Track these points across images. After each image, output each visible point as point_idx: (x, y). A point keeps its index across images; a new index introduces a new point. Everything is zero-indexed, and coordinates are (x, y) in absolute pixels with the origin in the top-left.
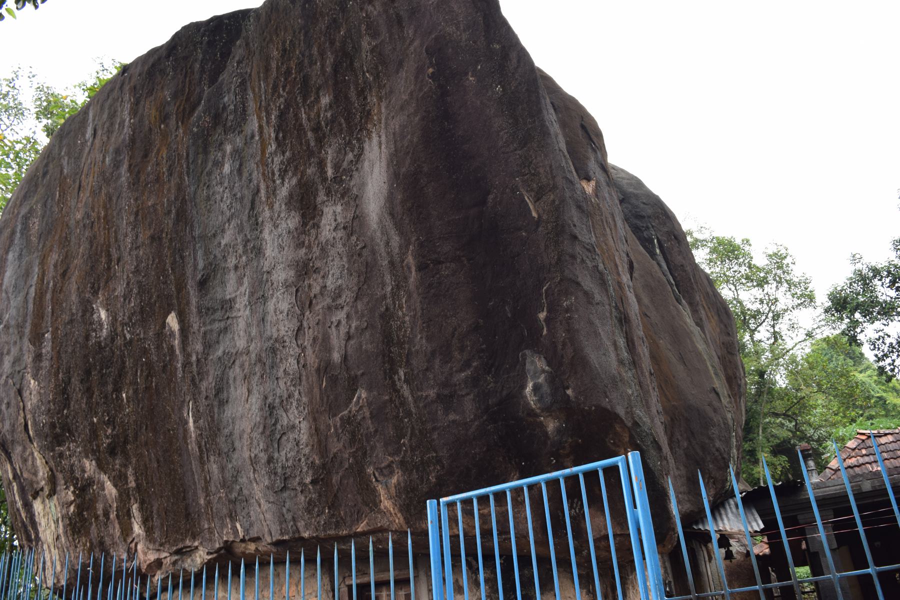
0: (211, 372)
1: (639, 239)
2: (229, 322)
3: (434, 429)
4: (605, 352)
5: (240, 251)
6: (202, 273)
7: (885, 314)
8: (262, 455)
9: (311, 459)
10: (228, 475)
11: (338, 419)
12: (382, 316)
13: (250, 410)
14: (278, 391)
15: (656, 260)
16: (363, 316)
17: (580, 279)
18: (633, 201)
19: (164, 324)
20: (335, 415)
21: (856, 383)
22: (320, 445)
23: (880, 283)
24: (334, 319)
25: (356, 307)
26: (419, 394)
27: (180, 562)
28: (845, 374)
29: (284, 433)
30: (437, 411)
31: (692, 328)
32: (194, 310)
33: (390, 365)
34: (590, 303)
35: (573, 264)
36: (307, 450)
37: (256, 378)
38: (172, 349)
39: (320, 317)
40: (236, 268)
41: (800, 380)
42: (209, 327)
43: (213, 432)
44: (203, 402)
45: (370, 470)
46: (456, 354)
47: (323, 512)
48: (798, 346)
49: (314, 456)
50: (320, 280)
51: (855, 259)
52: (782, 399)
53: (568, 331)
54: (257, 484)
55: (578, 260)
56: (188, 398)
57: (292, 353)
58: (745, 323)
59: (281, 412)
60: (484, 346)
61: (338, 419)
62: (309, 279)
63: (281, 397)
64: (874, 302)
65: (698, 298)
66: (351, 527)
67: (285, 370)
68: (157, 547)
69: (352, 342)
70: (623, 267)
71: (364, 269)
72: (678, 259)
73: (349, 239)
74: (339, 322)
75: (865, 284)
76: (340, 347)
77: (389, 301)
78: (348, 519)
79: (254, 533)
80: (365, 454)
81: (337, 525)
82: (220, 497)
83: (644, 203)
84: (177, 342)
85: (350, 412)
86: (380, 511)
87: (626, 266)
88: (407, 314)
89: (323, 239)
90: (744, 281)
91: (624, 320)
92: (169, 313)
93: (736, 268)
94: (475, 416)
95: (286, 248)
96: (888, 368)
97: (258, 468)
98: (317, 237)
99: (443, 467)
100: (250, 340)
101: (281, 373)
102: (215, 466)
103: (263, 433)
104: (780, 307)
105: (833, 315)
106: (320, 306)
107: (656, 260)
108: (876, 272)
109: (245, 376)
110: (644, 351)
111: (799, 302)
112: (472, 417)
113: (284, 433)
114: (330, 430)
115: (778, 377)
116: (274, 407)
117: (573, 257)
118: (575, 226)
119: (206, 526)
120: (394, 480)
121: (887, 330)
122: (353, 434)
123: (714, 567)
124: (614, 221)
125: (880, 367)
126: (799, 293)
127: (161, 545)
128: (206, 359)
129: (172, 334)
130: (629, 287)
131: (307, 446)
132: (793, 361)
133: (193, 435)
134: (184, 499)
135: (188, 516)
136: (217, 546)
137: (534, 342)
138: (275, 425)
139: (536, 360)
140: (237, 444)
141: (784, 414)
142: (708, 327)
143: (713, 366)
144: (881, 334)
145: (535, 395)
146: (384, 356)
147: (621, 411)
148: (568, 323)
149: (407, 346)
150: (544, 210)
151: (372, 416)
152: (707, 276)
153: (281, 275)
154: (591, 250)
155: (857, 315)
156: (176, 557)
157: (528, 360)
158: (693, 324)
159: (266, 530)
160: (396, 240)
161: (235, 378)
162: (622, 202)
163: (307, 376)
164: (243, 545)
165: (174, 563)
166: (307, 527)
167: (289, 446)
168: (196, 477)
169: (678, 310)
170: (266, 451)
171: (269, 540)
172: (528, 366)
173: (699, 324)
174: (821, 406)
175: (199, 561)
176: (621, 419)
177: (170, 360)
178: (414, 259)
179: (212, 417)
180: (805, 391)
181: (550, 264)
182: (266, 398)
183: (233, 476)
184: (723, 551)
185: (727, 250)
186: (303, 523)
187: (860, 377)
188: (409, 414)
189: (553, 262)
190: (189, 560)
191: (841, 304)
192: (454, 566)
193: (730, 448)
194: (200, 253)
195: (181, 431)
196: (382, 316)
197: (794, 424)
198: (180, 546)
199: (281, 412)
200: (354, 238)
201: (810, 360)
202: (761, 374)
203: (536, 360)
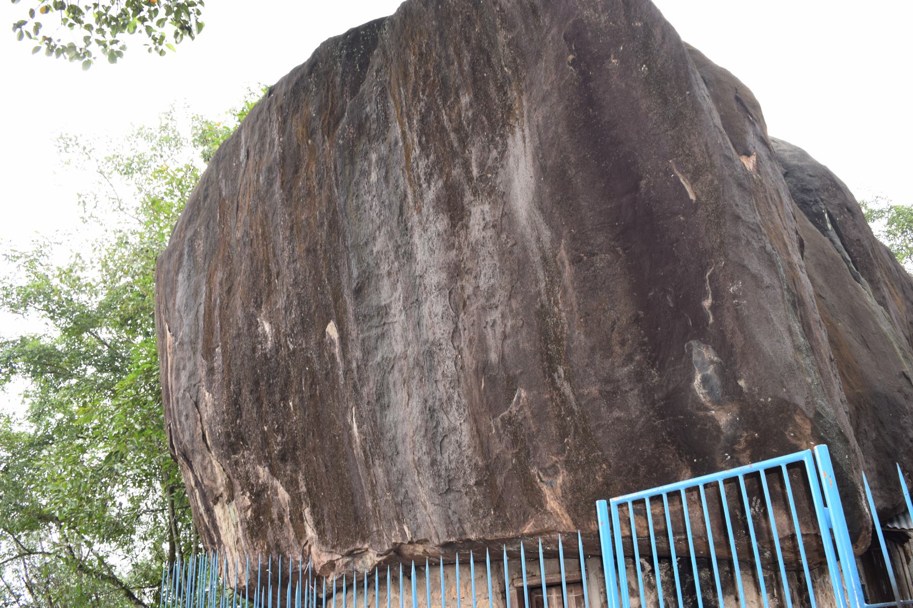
0: (372, 378)
1: (807, 214)
2: (386, 327)
3: (599, 427)
4: (779, 339)
5: (392, 258)
8: (425, 457)
10: (393, 479)
12: (538, 314)
13: (411, 413)
14: (438, 394)
17: (746, 262)
18: (798, 174)
19: (324, 333)
22: (482, 447)
24: (489, 319)
25: (511, 306)
26: (581, 391)
27: (352, 564)
29: (446, 436)
31: (874, 308)
32: (352, 318)
33: (550, 363)
35: (737, 246)
36: (469, 452)
37: (415, 382)
38: (333, 357)
40: (389, 274)
43: (376, 436)
44: (365, 408)
45: (534, 471)
46: (617, 349)
49: (477, 458)
53: (737, 318)
55: (743, 242)
57: (449, 355)
59: (441, 415)
60: (646, 339)
61: (498, 420)
62: (462, 280)
63: (440, 400)
65: (879, 274)
66: (517, 529)
69: (509, 341)
71: (516, 266)
72: (853, 233)
73: (499, 237)
74: (494, 322)
76: (497, 347)
77: (544, 297)
78: (515, 520)
79: (421, 536)
81: (504, 527)
82: (387, 501)
83: (811, 176)
84: (337, 350)
86: (546, 512)
87: (796, 245)
88: (565, 309)
89: (472, 239)
91: (797, 303)
94: (641, 412)
95: (437, 251)
97: (421, 471)
98: (466, 238)
99: (609, 466)
100: (407, 344)
101: (439, 376)
102: (380, 470)
103: (425, 436)
106: (474, 307)
107: (828, 236)
110: (821, 335)
112: (638, 413)
114: (491, 431)
116: (434, 410)
117: (737, 238)
118: (737, 205)
119: (375, 529)
120: (560, 480)
122: (515, 434)
124: (780, 197)
127: (333, 547)
128: (365, 365)
129: (332, 342)
130: (801, 267)
133: (358, 440)
134: (353, 502)
135: (356, 518)
136: (387, 548)
137: (700, 331)
138: (436, 427)
139: (704, 351)
140: (400, 448)
142: (892, 305)
143: (901, 349)
145: (704, 388)
146: (542, 354)
147: (800, 401)
148: (736, 310)
149: (565, 342)
150: (702, 192)
151: (534, 416)
152: (888, 251)
153: (434, 278)
154: (756, 229)
157: (695, 351)
159: (433, 532)
160: (546, 235)
162: (786, 175)
163: (465, 377)
164: (411, 547)
165: (347, 565)
166: (473, 528)
167: (451, 448)
168: (363, 481)
171: (436, 542)
172: (695, 357)
173: (882, 302)
176: (801, 410)
178: (567, 253)
179: (375, 422)
182: (426, 401)
188: (571, 412)
189: (716, 246)
190: (360, 562)
196: (538, 314)
198: (351, 548)
199: (441, 415)
203: (704, 351)
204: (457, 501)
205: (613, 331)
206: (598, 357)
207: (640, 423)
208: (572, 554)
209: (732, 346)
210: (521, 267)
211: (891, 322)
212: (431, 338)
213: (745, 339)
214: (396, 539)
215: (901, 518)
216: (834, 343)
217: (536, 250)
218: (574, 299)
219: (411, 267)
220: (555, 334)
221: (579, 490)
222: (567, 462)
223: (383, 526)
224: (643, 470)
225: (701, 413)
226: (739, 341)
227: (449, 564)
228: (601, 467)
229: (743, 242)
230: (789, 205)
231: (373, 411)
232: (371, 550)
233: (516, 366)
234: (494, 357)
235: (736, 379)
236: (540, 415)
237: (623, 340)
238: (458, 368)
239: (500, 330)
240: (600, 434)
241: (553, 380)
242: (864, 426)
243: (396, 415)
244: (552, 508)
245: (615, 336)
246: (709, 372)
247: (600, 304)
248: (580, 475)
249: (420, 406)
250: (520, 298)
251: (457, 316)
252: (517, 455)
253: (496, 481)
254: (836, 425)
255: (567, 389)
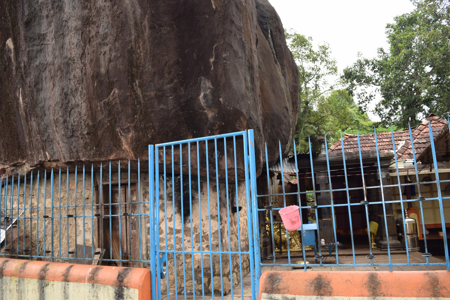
0: (33, 73)
1: (261, 28)
2: (43, 46)
3: (152, 112)
4: (240, 82)
5: (50, 7)
6: (27, 17)
7: (367, 82)
8: (60, 118)
9: (87, 122)
10: (42, 128)
11: (102, 103)
12: (129, 51)
13: (54, 95)
14: (70, 86)
15: (268, 40)
16: (118, 50)
17: (232, 44)
18: (261, 8)
19: (4, 45)
20: (100, 101)
21: (348, 113)
22: (92, 115)
23: (368, 67)
24: (102, 50)
25: (115, 45)
26: (146, 93)
27: (15, 171)
28: (344, 108)
29: (73, 108)
30: (154, 103)
31: (280, 77)
32: (23, 38)
33: (132, 78)
34: (236, 57)
35: (230, 36)
36: (85, 118)
37: (58, 78)
38: (9, 58)
39: (95, 48)
40: (47, 16)
41: (324, 109)
42: (31, 49)
43: (34, 106)
44: (27, 89)
45: (118, 129)
46: (166, 75)
47: (92, 149)
48: (326, 92)
49: (89, 121)
50: (96, 29)
51: (359, 54)
52: (314, 116)
53: (224, 69)
54: (58, 133)
55: (233, 34)
56: (19, 86)
57: (78, 66)
58: (304, 79)
59: (71, 97)
60: (181, 73)
61: (102, 103)
62: (90, 27)
63: (71, 89)
64: (363, 76)
65: (285, 62)
66: (106, 157)
67: (74, 75)
68: (2, 162)
69: (112, 64)
70: (254, 41)
71: (120, 24)
72: (279, 42)
73: (113, 7)
74: (105, 52)
75: (361, 67)
76: (105, 66)
77: (133, 44)
78: (106, 152)
79: (55, 158)
80: (116, 122)
81: (100, 155)
82: (37, 139)
83: (267, 10)
84: (12, 55)
85: (109, 100)
86: (122, 150)
87: (255, 41)
88: (143, 51)
89: (98, 6)
90: (306, 57)
91: (251, 68)
92: (8, 38)
93: (304, 51)
94: (174, 107)
95: (77, 8)
96: (363, 108)
97: (58, 125)
98: (94, 4)
99: (155, 131)
100: (55, 57)
101: (72, 77)
102: (34, 123)
103: (61, 107)
104: (320, 73)
105: (344, 80)
106: (95, 43)
107: (268, 40)
108: (367, 62)
109: (52, 77)
110: (258, 84)
111: (330, 71)
112: (172, 107)
113: (73, 108)
114: (98, 108)
115: (314, 106)
116: (67, 95)
117: (231, 32)
118: (233, 16)
119: (30, 153)
120: (130, 135)
121: (366, 90)
122: (110, 111)
123: (273, 188)
124: (252, 17)
125: (360, 107)
126: (331, 67)
127: (5, 161)
128: (29, 66)
129: (9, 50)
130: (255, 51)
131: (85, 115)
132: (323, 98)
133: (22, 106)
134: (17, 139)
135: (19, 147)
136: (36, 163)
137: (206, 73)
138: (68, 103)
140: (47, 112)
141: (314, 123)
142: (288, 77)
143: (287, 96)
144: (363, 91)
145: (204, 99)
146: (128, 72)
147: (244, 111)
148: (224, 66)
149: (141, 68)
150: (219, 5)
151: (121, 103)
152: (291, 53)
153: (74, 23)
154: (240, 29)
155: (355, 82)
156: (13, 168)
157: (202, 82)
158: (281, 75)
159: (62, 156)
160: (139, 11)
161: (46, 77)
162: (256, 7)
163: (86, 79)
164: (50, 163)
165: (12, 171)
166: (84, 155)
167: (75, 115)
168: (24, 128)
169: (275, 67)
170: (63, 116)
171: (64, 161)
172: (202, 85)
173: (284, 75)
174: (331, 121)
175: (26, 170)
176: (244, 115)
177: (8, 65)
178: (148, 23)
179: (33, 97)
180: (326, 114)
181: (219, 34)
182: (63, 89)
183: (44, 129)
184: (279, 181)
185: (301, 41)
186: (82, 154)
187: (350, 110)
188: (139, 103)
189: (221, 33)
190: (20, 170)
191: (349, 75)
192: (160, 174)
193: (289, 135)
194: (26, 6)
195: (15, 103)
196: (129, 51)
197: (317, 128)
198: (15, 162)
199: (71, 97)
200: (116, 7)
201: (330, 100)
202: (307, 103)
204: (76, 141)
205: (165, 66)
206: (156, 78)
207: (172, 112)
208: (134, 171)
209: (220, 82)
210: (123, 25)
211: (286, 84)
212: (69, 56)
213: (226, 79)
214: (41, 158)
215: (273, 166)
216: (262, 89)
217: (132, 18)
218: (149, 47)
219: (61, 14)
220: (137, 63)
221: (139, 140)
222: (135, 127)
223: (35, 152)
224: (170, 134)
225: (201, 111)
226: (223, 80)
227: (72, 172)
228: (151, 131)
229: (233, 34)
230: (255, 23)
231: (32, 92)
232: (27, 164)
233: (114, 77)
234: (103, 70)
235: (219, 97)
236: (124, 102)
237: (170, 71)
238: (83, 74)
239: (107, 56)
240: (152, 115)
241: (133, 87)
242: (267, 126)
243: (45, 95)
244: (125, 148)
245: (166, 68)
246: (207, 92)
247: (161, 52)
248: (141, 134)
249: (59, 91)
250: (120, 42)
251: (85, 46)
252: (110, 121)
253: (98, 133)
254: (257, 124)
255: (139, 91)
